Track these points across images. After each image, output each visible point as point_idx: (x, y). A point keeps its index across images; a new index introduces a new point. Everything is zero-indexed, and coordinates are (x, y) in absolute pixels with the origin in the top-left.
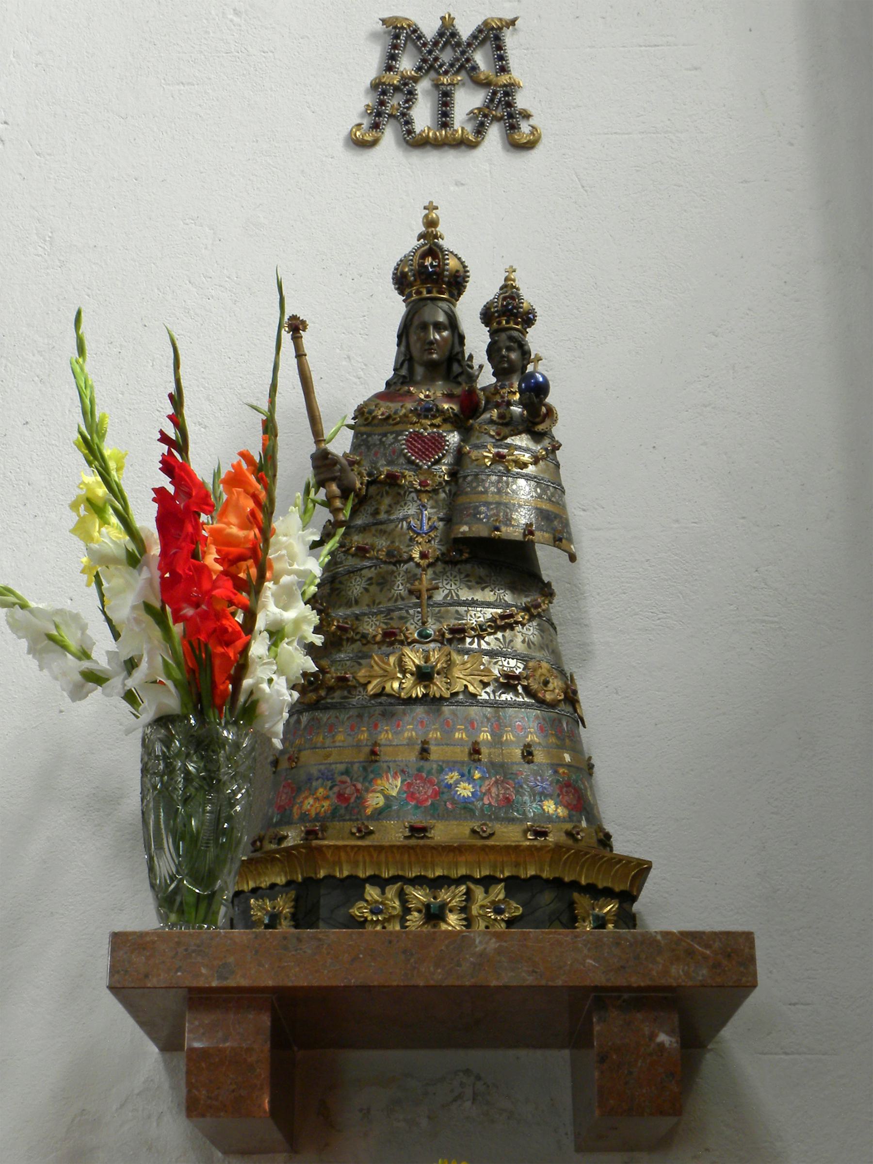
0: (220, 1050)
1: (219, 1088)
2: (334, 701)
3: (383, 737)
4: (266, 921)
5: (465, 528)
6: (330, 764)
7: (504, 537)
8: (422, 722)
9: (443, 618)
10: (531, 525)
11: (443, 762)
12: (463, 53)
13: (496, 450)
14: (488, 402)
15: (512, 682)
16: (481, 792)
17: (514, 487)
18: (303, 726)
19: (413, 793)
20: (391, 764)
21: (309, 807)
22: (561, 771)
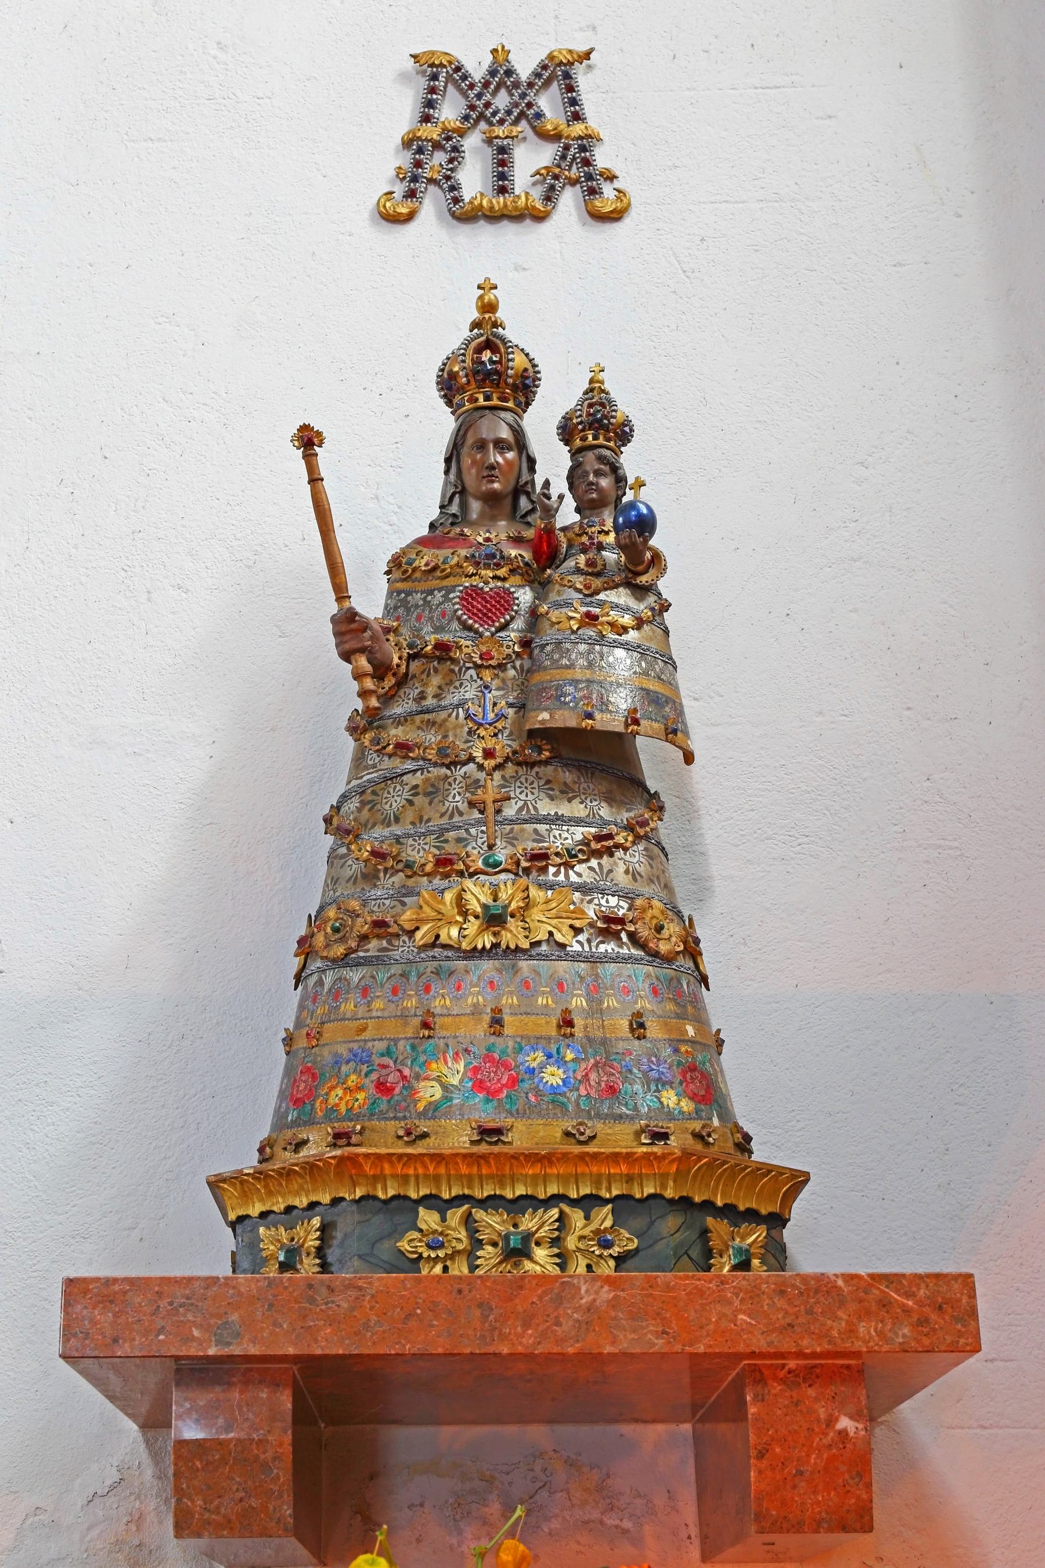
0: (221, 1443)
1: (220, 1497)
2: (368, 954)
3: (437, 1006)
4: (282, 1258)
5: (545, 716)
6: (365, 1041)
7: (599, 726)
8: (491, 983)
9: (517, 839)
10: (635, 710)
11: (522, 1037)
12: (523, 96)
13: (584, 609)
14: (570, 546)
15: (613, 926)
16: (575, 1078)
17: (611, 659)
18: (326, 987)
19: (481, 1081)
20: (451, 1042)
21: (337, 1101)
22: (683, 1049)
